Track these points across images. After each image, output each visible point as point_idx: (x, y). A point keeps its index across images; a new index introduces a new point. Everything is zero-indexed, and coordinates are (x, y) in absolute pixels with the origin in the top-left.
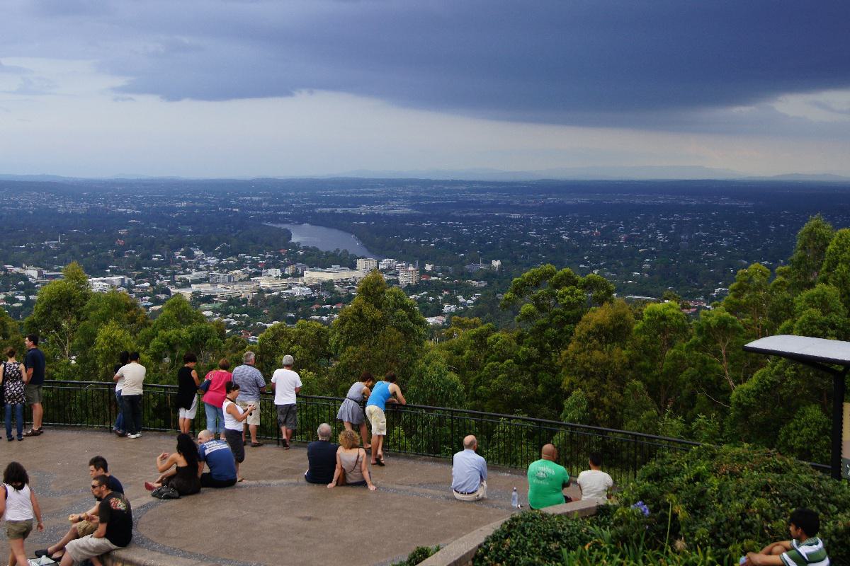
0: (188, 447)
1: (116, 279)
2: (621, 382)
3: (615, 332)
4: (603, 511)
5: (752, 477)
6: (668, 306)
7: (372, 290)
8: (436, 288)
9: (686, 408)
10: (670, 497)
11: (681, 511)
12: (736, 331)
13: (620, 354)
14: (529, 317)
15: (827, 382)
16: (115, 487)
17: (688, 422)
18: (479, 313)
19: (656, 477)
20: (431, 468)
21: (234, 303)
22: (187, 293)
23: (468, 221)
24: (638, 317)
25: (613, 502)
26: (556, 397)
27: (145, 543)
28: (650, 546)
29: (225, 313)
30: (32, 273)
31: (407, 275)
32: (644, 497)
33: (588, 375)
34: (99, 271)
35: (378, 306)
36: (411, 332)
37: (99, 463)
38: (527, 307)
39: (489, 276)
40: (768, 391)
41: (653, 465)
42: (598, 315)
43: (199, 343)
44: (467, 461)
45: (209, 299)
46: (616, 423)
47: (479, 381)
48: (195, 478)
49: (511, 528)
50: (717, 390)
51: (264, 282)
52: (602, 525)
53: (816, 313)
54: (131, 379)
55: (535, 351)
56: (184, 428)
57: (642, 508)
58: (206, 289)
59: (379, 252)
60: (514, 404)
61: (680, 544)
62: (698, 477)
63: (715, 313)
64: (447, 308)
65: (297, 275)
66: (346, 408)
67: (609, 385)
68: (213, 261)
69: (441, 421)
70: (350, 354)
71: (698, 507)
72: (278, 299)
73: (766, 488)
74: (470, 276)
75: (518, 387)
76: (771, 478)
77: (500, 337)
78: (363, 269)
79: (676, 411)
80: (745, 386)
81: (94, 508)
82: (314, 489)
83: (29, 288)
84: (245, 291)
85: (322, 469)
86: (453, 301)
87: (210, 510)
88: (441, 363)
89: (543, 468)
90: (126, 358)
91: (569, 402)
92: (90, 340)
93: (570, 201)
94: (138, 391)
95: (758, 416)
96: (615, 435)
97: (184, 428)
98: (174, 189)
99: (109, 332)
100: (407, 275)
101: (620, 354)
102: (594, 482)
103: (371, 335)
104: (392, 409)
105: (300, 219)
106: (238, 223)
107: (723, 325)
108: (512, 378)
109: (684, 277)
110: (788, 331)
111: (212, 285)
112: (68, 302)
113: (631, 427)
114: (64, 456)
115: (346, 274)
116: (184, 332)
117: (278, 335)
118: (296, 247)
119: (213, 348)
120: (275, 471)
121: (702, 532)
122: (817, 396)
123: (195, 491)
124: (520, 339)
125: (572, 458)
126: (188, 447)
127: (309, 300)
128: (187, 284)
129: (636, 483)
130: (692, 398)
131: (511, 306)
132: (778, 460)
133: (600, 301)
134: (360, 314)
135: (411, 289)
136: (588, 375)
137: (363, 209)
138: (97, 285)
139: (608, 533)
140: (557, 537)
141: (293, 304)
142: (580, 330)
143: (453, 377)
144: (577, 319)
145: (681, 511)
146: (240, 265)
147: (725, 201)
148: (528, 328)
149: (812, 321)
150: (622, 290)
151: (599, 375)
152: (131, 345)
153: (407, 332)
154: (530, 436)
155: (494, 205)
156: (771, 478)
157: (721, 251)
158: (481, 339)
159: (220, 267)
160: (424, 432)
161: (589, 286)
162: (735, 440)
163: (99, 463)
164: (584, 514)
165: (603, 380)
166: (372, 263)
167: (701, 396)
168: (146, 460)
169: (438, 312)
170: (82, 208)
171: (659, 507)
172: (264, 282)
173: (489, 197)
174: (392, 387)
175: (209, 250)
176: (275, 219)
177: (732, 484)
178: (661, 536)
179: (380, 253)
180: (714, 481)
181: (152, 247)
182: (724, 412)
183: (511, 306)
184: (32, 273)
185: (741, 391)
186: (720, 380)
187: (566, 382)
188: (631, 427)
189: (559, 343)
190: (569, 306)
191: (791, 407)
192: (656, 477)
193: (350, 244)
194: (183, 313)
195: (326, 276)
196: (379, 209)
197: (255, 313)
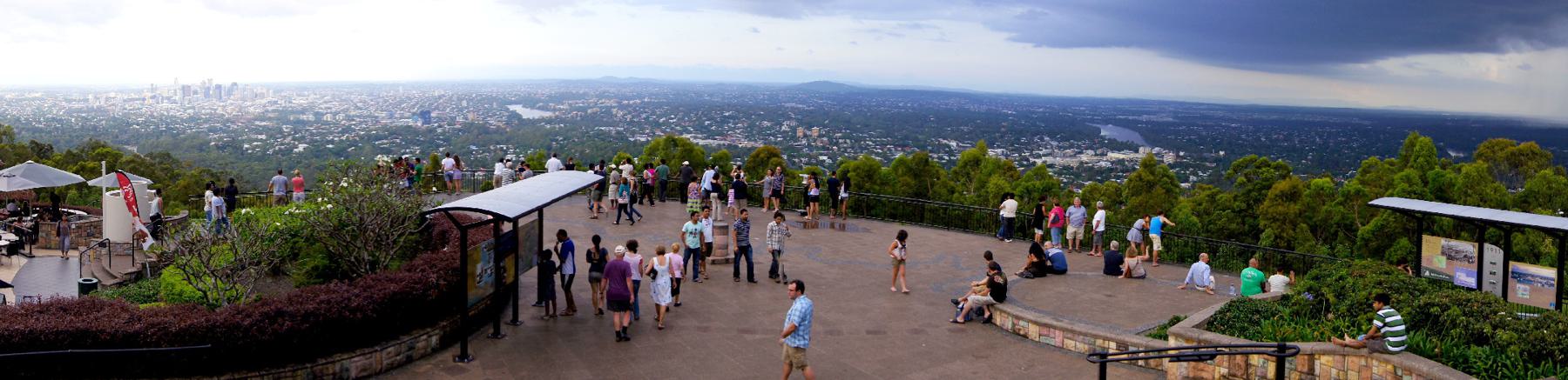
0: (1036, 250)
1: (999, 151)
2: (1294, 225)
3: (1292, 196)
4: (1285, 298)
5: (1372, 277)
6: (1324, 181)
7: (1148, 165)
8: (1187, 166)
9: (1330, 240)
10: (1324, 290)
11: (1332, 299)
12: (1365, 195)
13: (1294, 208)
14: (1242, 185)
15: (1412, 225)
16: (995, 267)
17: (1332, 248)
18: (1211, 182)
19: (1316, 278)
20: (1181, 269)
21: (1066, 169)
22: (1039, 162)
23: (1205, 127)
24: (1308, 187)
25: (1290, 293)
26: (1256, 233)
27: (1013, 302)
28: (1313, 317)
29: (1060, 174)
30: (953, 144)
31: (1169, 158)
32: (1309, 290)
33: (1275, 220)
34: (991, 145)
35: (1152, 173)
36: (1171, 192)
37: (989, 256)
38: (1241, 179)
39: (1218, 160)
40: (1380, 231)
41: (1314, 272)
42: (1282, 185)
43: (1046, 192)
44: (1201, 268)
45: (1051, 166)
46: (1290, 248)
47: (1210, 222)
48: (1042, 268)
49: (1231, 306)
50: (1350, 229)
51: (1084, 158)
52: (1285, 306)
53: (1406, 186)
54: (1009, 208)
55: (1244, 206)
56: (1037, 239)
57: (1310, 297)
58: (1049, 160)
59: (1153, 143)
60: (1231, 235)
61: (1330, 316)
62: (1341, 278)
63: (1352, 185)
64: (1192, 178)
65: (1103, 154)
66: (1133, 235)
67: (1288, 226)
68: (1054, 143)
69: (1186, 244)
70: (1134, 201)
71: (1340, 296)
72: (1092, 168)
73: (1380, 283)
74: (1206, 160)
75: (1234, 226)
76: (1383, 278)
77: (1224, 197)
78: (1143, 153)
79: (1325, 241)
80: (1367, 227)
81: (986, 280)
82: (1111, 279)
83: (951, 153)
84: (1073, 162)
85: (1113, 266)
86: (1195, 174)
87: (1050, 286)
88: (1187, 210)
89: (1251, 273)
90: (1004, 198)
91: (1263, 235)
92: (983, 185)
93: (1264, 117)
94: (1013, 215)
95: (1374, 244)
96: (1289, 256)
97: (1037, 239)
98: (1034, 102)
99: (996, 182)
100: (1169, 158)
101: (1294, 208)
102: (1278, 282)
103: (1150, 190)
104: (1165, 233)
105: (1106, 122)
106: (1071, 122)
107: (1358, 192)
108: (1230, 221)
109: (1331, 163)
110: (1392, 195)
111: (1053, 158)
112: (976, 162)
113: (1299, 250)
114: (974, 244)
115: (1132, 155)
116: (1038, 183)
117: (1092, 190)
118: (1103, 138)
119: (1056, 195)
120: (1088, 265)
121: (1343, 308)
122: (1406, 232)
123: (1043, 275)
124: (1235, 199)
125: (1267, 267)
126: (1036, 250)
127: (1111, 170)
128: (1039, 156)
129: (1306, 281)
130: (1336, 234)
131: (1231, 179)
132: (1387, 267)
133: (1284, 177)
134: (1140, 178)
135: (1171, 166)
136: (1275, 220)
137: (1145, 118)
138: (991, 152)
139: (1288, 311)
140: (1258, 312)
141: (1101, 171)
142: (1271, 193)
143: (1195, 219)
144: (1269, 187)
145: (1332, 299)
146: (1071, 146)
147: (1356, 121)
148: (1242, 191)
149: (1404, 190)
150: (1295, 171)
151: (1282, 220)
152: (1008, 190)
153: (1168, 191)
154: (1240, 255)
155: (1222, 119)
156: (1383, 278)
157: (1353, 150)
158: (1212, 197)
159: (1059, 148)
160: (1179, 252)
161: (1277, 168)
162: (1361, 257)
163: (989, 256)
164: (1275, 300)
165: (1284, 222)
166: (1148, 150)
167: (1341, 234)
168: (1015, 257)
169: (1187, 181)
170: (984, 108)
171: (1318, 295)
172: (1084, 158)
173: (1220, 114)
174: (1162, 219)
175: (1053, 138)
176: (1092, 121)
177: (1361, 282)
178: (1319, 311)
179: (1153, 144)
180: (1350, 280)
181: (1021, 133)
182: (1354, 242)
183: (1231, 179)
184: (953, 144)
185: (1364, 230)
186: (1352, 223)
187: (1262, 223)
188: (1299, 250)
189: (1258, 201)
190: (1266, 179)
191: (1391, 238)
192: (1316, 278)
193: (1135, 137)
194: (1040, 173)
195: (1121, 156)
196: (1153, 118)
197: (1078, 176)
